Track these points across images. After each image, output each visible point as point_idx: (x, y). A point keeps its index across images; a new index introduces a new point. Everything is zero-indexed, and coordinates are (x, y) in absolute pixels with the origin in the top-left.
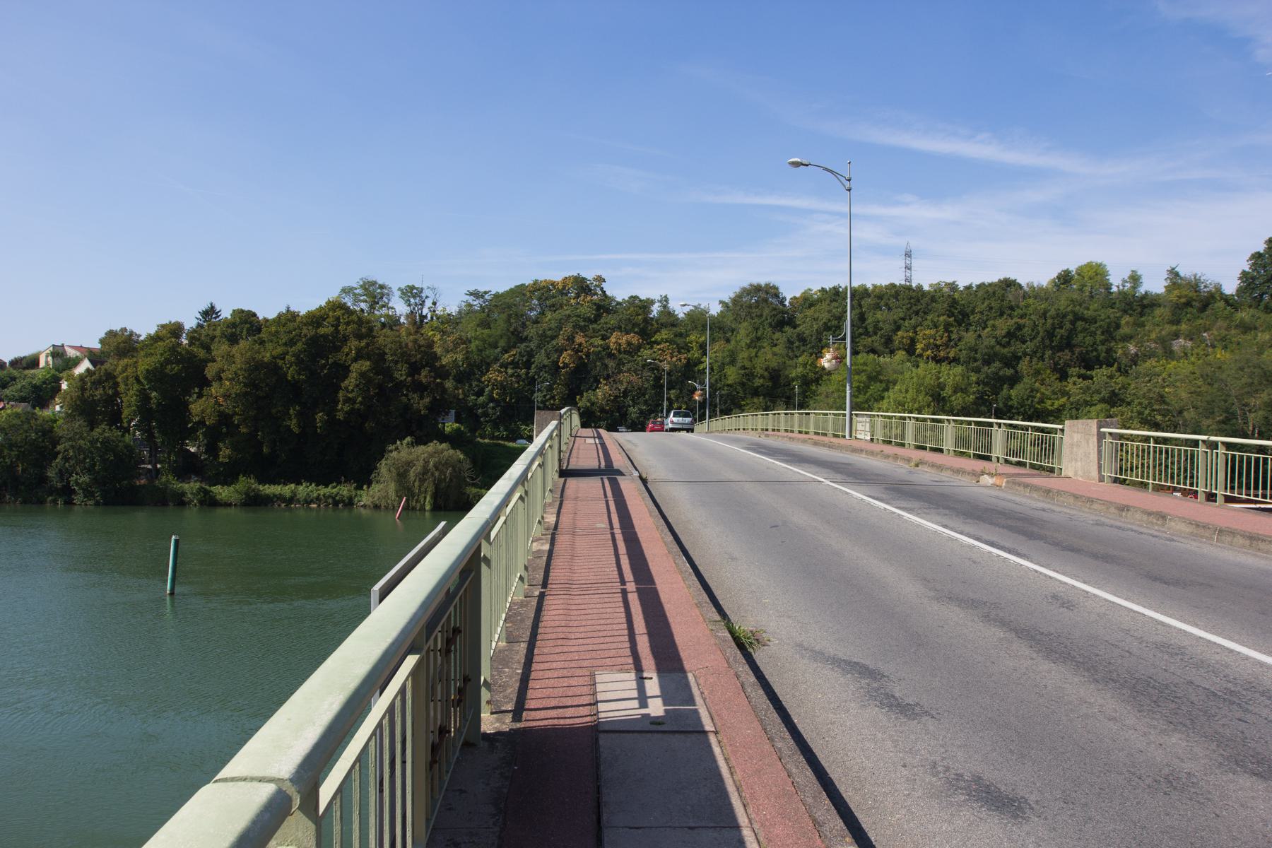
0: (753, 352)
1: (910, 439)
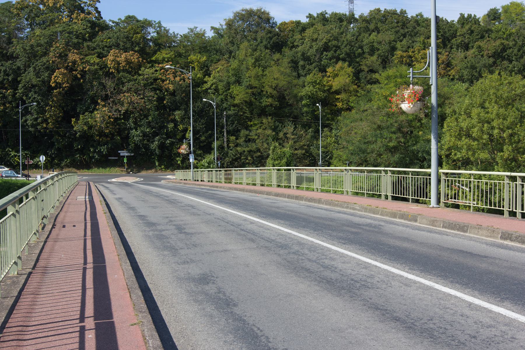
1: (274, 182)
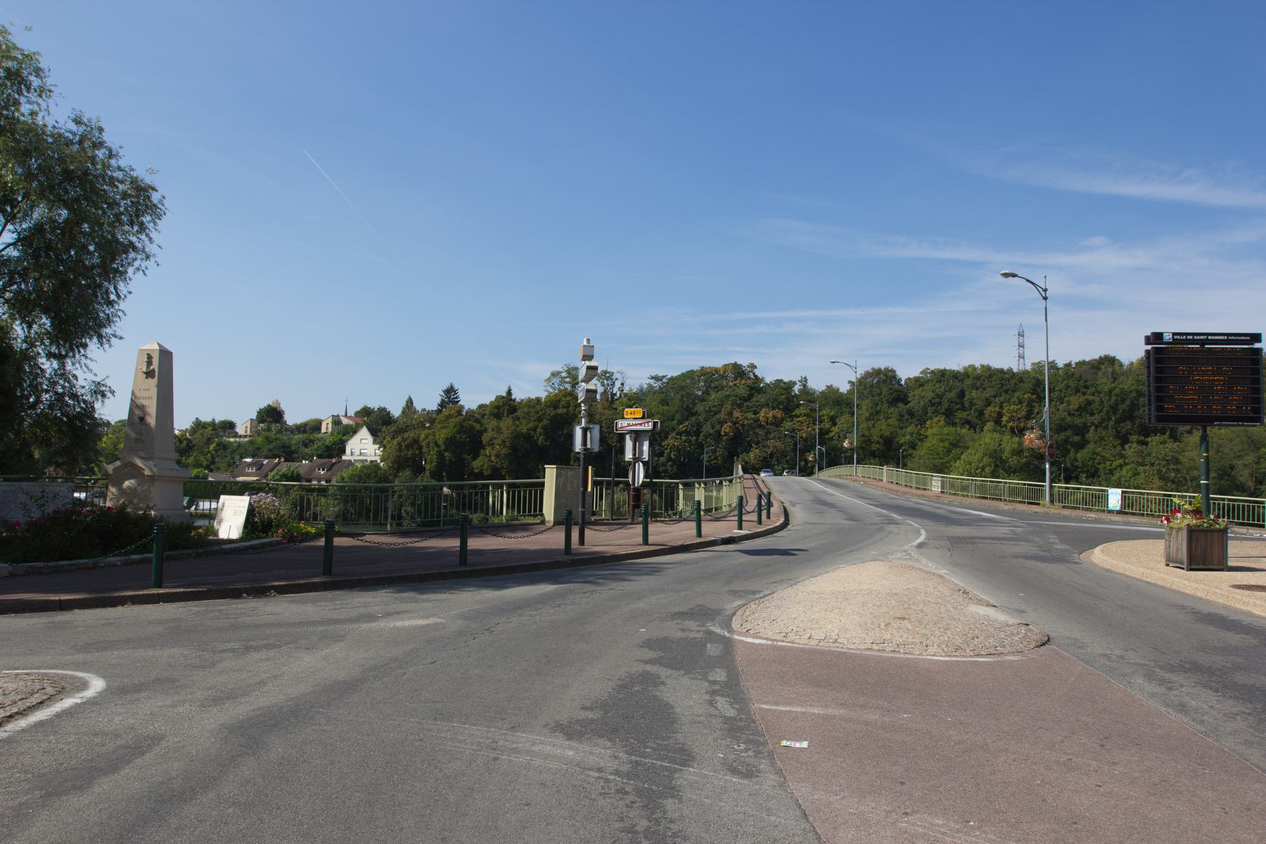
0: (871, 423)
